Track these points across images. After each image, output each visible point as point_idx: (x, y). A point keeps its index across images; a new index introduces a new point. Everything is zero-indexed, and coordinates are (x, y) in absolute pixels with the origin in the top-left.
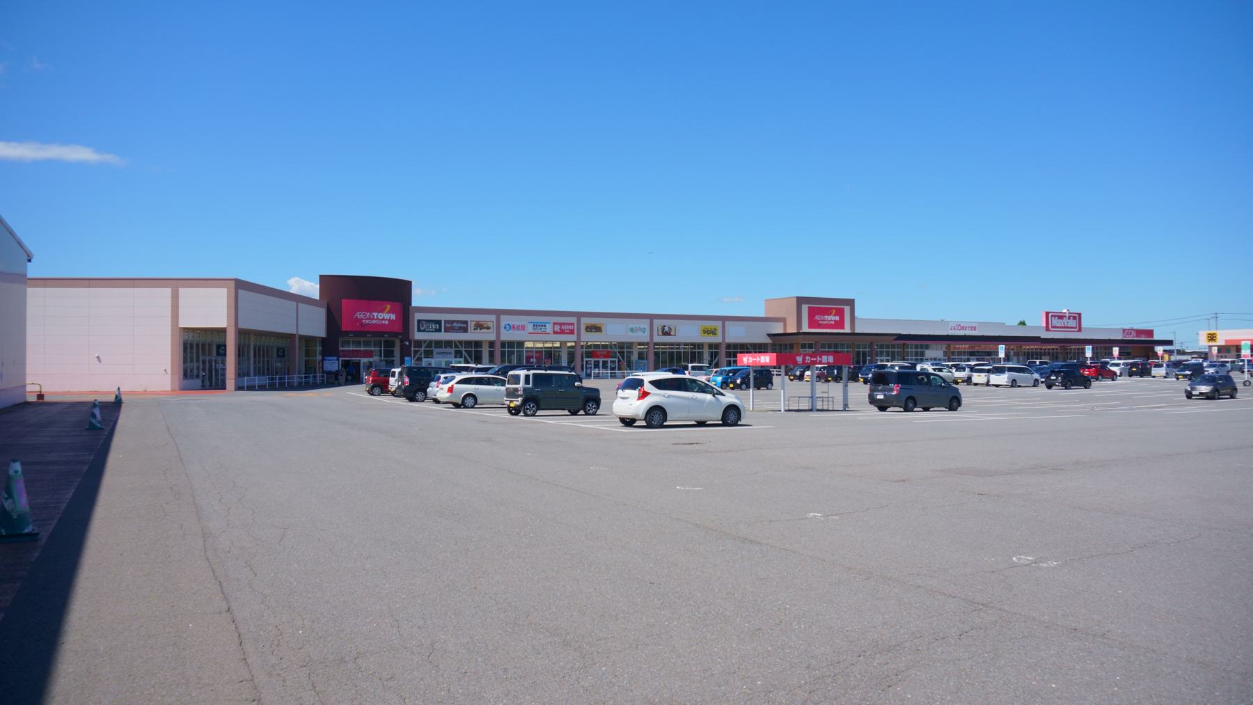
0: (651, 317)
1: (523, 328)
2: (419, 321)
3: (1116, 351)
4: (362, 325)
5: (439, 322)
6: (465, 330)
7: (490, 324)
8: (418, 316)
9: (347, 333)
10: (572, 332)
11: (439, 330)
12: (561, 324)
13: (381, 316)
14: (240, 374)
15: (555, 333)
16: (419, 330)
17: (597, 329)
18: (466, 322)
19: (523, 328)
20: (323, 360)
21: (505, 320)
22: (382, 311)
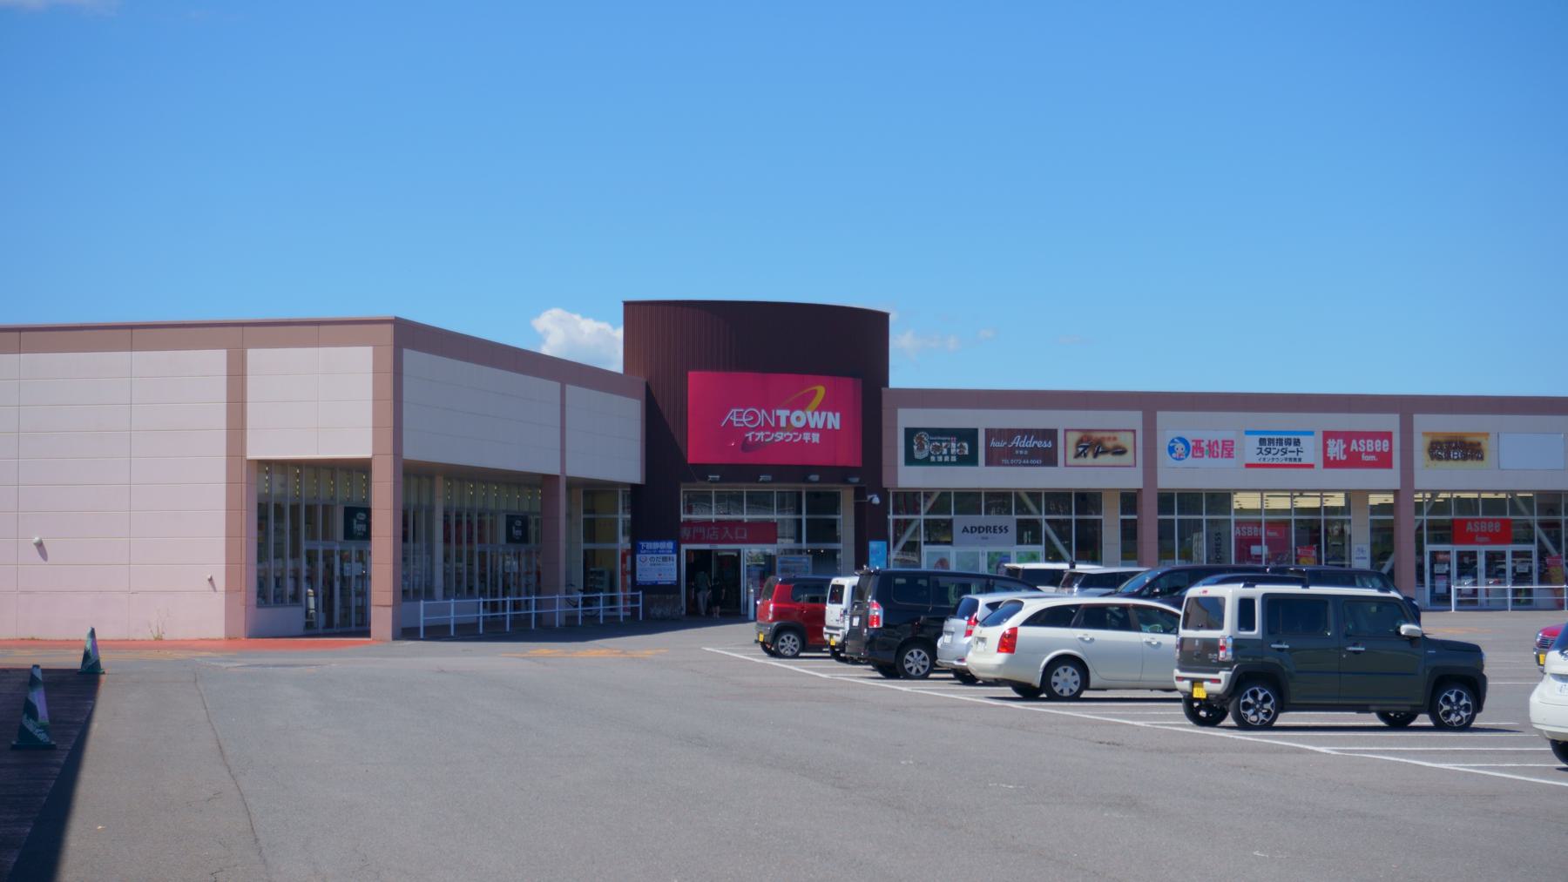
1: (1227, 449)
2: (910, 433)
4: (746, 446)
5: (969, 435)
6: (1049, 458)
7: (1125, 440)
8: (908, 418)
10: (1384, 461)
11: (970, 460)
12: (1348, 437)
13: (799, 418)
15: (1329, 463)
16: (910, 460)
17: (1468, 449)
18: (1050, 435)
19: (1227, 449)
20: (635, 550)
21: (1170, 425)
22: (802, 404)
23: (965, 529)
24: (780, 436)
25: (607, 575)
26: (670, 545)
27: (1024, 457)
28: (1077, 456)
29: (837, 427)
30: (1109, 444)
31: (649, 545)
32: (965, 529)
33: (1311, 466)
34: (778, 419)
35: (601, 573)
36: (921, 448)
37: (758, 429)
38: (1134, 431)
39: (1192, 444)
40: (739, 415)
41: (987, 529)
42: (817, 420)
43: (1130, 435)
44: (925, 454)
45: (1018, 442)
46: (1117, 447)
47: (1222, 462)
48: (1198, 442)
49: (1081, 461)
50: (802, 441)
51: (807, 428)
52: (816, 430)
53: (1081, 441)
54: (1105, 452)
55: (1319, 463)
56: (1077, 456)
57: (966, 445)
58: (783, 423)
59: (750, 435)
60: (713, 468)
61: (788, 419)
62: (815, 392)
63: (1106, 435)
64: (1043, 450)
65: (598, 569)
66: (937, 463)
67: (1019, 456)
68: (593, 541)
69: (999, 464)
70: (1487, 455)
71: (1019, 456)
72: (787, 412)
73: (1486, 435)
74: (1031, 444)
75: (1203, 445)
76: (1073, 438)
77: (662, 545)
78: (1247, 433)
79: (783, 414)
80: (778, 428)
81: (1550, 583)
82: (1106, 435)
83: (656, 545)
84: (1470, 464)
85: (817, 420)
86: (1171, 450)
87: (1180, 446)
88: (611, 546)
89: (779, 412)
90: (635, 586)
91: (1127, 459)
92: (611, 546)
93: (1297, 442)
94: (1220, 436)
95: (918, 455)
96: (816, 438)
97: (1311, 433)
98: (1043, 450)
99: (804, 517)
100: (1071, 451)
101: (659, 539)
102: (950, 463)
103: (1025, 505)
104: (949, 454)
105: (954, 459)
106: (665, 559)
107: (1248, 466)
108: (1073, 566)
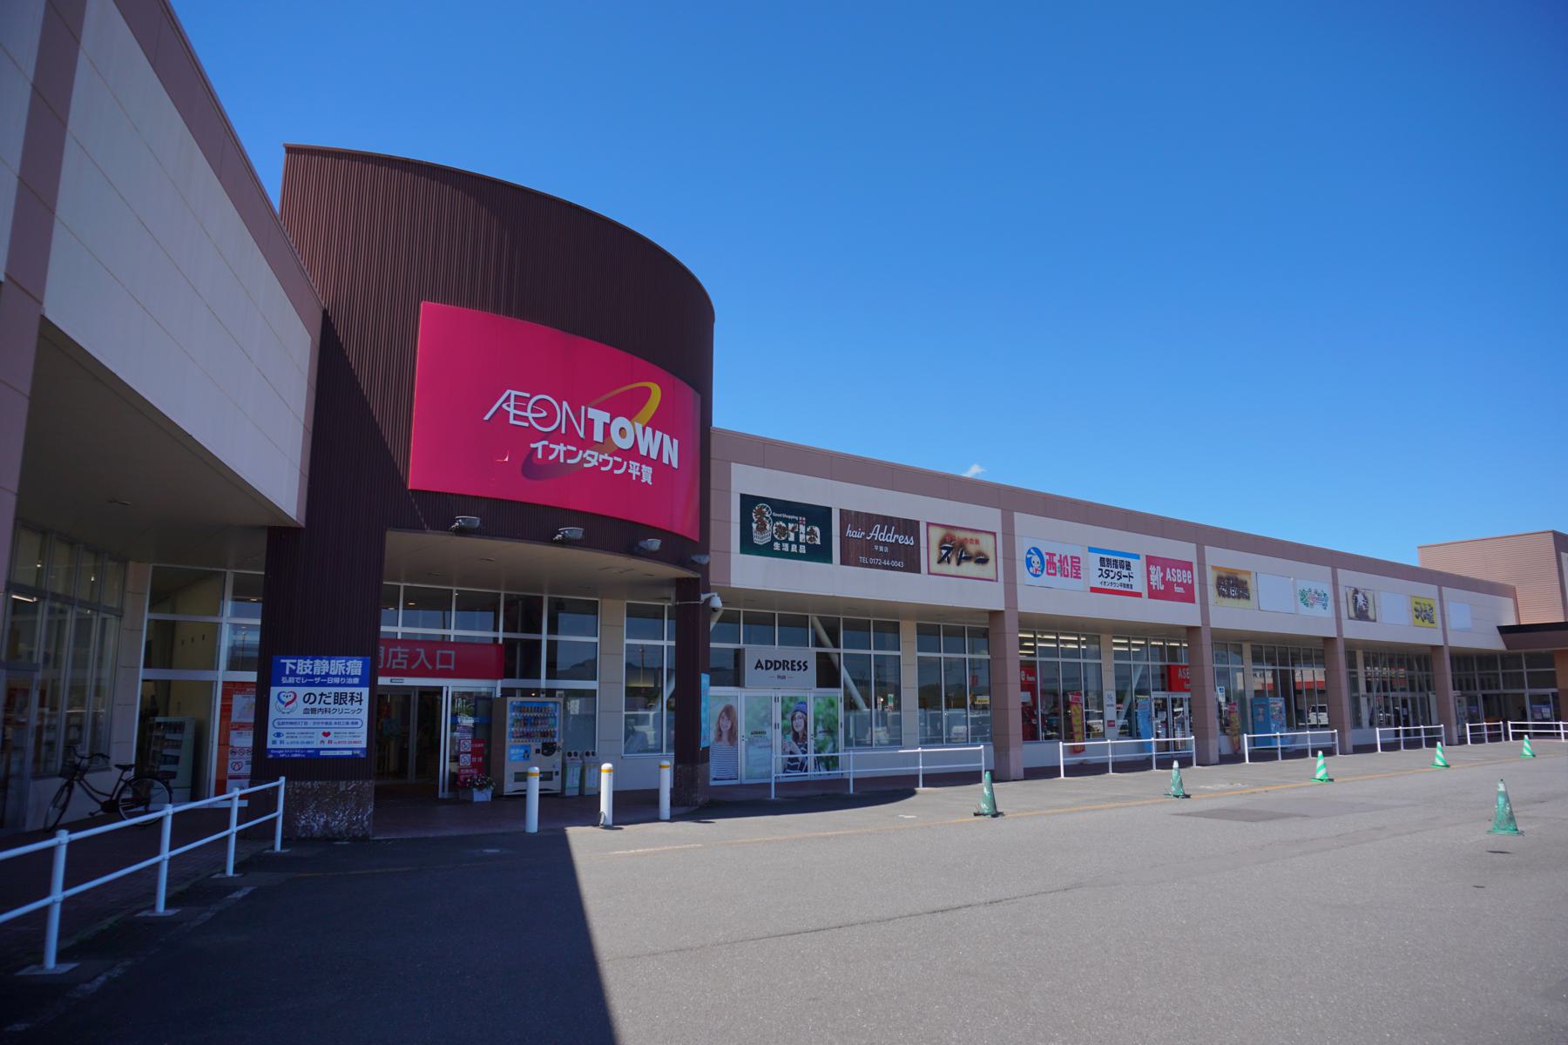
0: (1335, 560)
1: (1072, 567)
2: (748, 502)
3: (1176, 764)
4: (531, 467)
5: (818, 516)
6: (909, 561)
7: (986, 545)
8: (746, 479)
9: (436, 511)
10: (1188, 597)
11: (820, 553)
12: (1165, 564)
13: (628, 432)
14: (157, 621)
15: (1154, 594)
16: (748, 546)
17: (1233, 586)
18: (910, 527)
19: (1072, 567)
20: (269, 676)
21: (1033, 532)
22: (627, 407)
23: (759, 665)
24: (592, 458)
25: (188, 737)
26: (355, 666)
27: (884, 556)
28: (940, 561)
29: (675, 465)
30: (972, 549)
31: (304, 666)
32: (759, 665)
33: (1139, 595)
34: (590, 424)
35: (178, 727)
36: (762, 529)
37: (555, 437)
38: (994, 534)
39: (1046, 557)
40: (521, 403)
41: (784, 664)
42: (650, 443)
43: (991, 538)
44: (768, 539)
45: (877, 534)
46: (980, 553)
47: (1070, 582)
48: (1052, 555)
49: (944, 568)
50: (627, 474)
51: (632, 453)
52: (646, 460)
53: (943, 541)
54: (968, 559)
55: (1145, 594)
56: (940, 561)
57: (811, 530)
58: (598, 436)
59: (539, 445)
60: (469, 503)
61: (607, 427)
62: (647, 393)
63: (969, 535)
64: (896, 547)
65: (173, 719)
66: (782, 554)
67: (878, 554)
68: (168, 664)
69: (858, 564)
70: (1252, 595)
71: (878, 554)
72: (606, 416)
73: (1249, 573)
74: (891, 538)
75: (1056, 559)
76: (937, 534)
77: (336, 666)
78: (1091, 550)
79: (599, 417)
80: (588, 443)
81: (1138, 736)
82: (969, 535)
83: (321, 666)
84: (1242, 602)
85: (650, 443)
86: (1029, 563)
87: (1036, 559)
88: (206, 676)
89: (593, 413)
90: (265, 764)
91: (987, 570)
92: (206, 676)
93: (1128, 566)
94: (1069, 551)
95: (759, 539)
96: (647, 474)
97: (1137, 557)
98: (896, 547)
99: (544, 637)
100: (934, 556)
101: (330, 653)
102: (797, 556)
103: (828, 633)
104: (797, 541)
105: (803, 550)
106: (340, 699)
107: (1093, 590)
108: (776, 726)
